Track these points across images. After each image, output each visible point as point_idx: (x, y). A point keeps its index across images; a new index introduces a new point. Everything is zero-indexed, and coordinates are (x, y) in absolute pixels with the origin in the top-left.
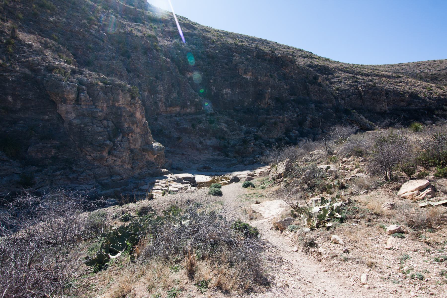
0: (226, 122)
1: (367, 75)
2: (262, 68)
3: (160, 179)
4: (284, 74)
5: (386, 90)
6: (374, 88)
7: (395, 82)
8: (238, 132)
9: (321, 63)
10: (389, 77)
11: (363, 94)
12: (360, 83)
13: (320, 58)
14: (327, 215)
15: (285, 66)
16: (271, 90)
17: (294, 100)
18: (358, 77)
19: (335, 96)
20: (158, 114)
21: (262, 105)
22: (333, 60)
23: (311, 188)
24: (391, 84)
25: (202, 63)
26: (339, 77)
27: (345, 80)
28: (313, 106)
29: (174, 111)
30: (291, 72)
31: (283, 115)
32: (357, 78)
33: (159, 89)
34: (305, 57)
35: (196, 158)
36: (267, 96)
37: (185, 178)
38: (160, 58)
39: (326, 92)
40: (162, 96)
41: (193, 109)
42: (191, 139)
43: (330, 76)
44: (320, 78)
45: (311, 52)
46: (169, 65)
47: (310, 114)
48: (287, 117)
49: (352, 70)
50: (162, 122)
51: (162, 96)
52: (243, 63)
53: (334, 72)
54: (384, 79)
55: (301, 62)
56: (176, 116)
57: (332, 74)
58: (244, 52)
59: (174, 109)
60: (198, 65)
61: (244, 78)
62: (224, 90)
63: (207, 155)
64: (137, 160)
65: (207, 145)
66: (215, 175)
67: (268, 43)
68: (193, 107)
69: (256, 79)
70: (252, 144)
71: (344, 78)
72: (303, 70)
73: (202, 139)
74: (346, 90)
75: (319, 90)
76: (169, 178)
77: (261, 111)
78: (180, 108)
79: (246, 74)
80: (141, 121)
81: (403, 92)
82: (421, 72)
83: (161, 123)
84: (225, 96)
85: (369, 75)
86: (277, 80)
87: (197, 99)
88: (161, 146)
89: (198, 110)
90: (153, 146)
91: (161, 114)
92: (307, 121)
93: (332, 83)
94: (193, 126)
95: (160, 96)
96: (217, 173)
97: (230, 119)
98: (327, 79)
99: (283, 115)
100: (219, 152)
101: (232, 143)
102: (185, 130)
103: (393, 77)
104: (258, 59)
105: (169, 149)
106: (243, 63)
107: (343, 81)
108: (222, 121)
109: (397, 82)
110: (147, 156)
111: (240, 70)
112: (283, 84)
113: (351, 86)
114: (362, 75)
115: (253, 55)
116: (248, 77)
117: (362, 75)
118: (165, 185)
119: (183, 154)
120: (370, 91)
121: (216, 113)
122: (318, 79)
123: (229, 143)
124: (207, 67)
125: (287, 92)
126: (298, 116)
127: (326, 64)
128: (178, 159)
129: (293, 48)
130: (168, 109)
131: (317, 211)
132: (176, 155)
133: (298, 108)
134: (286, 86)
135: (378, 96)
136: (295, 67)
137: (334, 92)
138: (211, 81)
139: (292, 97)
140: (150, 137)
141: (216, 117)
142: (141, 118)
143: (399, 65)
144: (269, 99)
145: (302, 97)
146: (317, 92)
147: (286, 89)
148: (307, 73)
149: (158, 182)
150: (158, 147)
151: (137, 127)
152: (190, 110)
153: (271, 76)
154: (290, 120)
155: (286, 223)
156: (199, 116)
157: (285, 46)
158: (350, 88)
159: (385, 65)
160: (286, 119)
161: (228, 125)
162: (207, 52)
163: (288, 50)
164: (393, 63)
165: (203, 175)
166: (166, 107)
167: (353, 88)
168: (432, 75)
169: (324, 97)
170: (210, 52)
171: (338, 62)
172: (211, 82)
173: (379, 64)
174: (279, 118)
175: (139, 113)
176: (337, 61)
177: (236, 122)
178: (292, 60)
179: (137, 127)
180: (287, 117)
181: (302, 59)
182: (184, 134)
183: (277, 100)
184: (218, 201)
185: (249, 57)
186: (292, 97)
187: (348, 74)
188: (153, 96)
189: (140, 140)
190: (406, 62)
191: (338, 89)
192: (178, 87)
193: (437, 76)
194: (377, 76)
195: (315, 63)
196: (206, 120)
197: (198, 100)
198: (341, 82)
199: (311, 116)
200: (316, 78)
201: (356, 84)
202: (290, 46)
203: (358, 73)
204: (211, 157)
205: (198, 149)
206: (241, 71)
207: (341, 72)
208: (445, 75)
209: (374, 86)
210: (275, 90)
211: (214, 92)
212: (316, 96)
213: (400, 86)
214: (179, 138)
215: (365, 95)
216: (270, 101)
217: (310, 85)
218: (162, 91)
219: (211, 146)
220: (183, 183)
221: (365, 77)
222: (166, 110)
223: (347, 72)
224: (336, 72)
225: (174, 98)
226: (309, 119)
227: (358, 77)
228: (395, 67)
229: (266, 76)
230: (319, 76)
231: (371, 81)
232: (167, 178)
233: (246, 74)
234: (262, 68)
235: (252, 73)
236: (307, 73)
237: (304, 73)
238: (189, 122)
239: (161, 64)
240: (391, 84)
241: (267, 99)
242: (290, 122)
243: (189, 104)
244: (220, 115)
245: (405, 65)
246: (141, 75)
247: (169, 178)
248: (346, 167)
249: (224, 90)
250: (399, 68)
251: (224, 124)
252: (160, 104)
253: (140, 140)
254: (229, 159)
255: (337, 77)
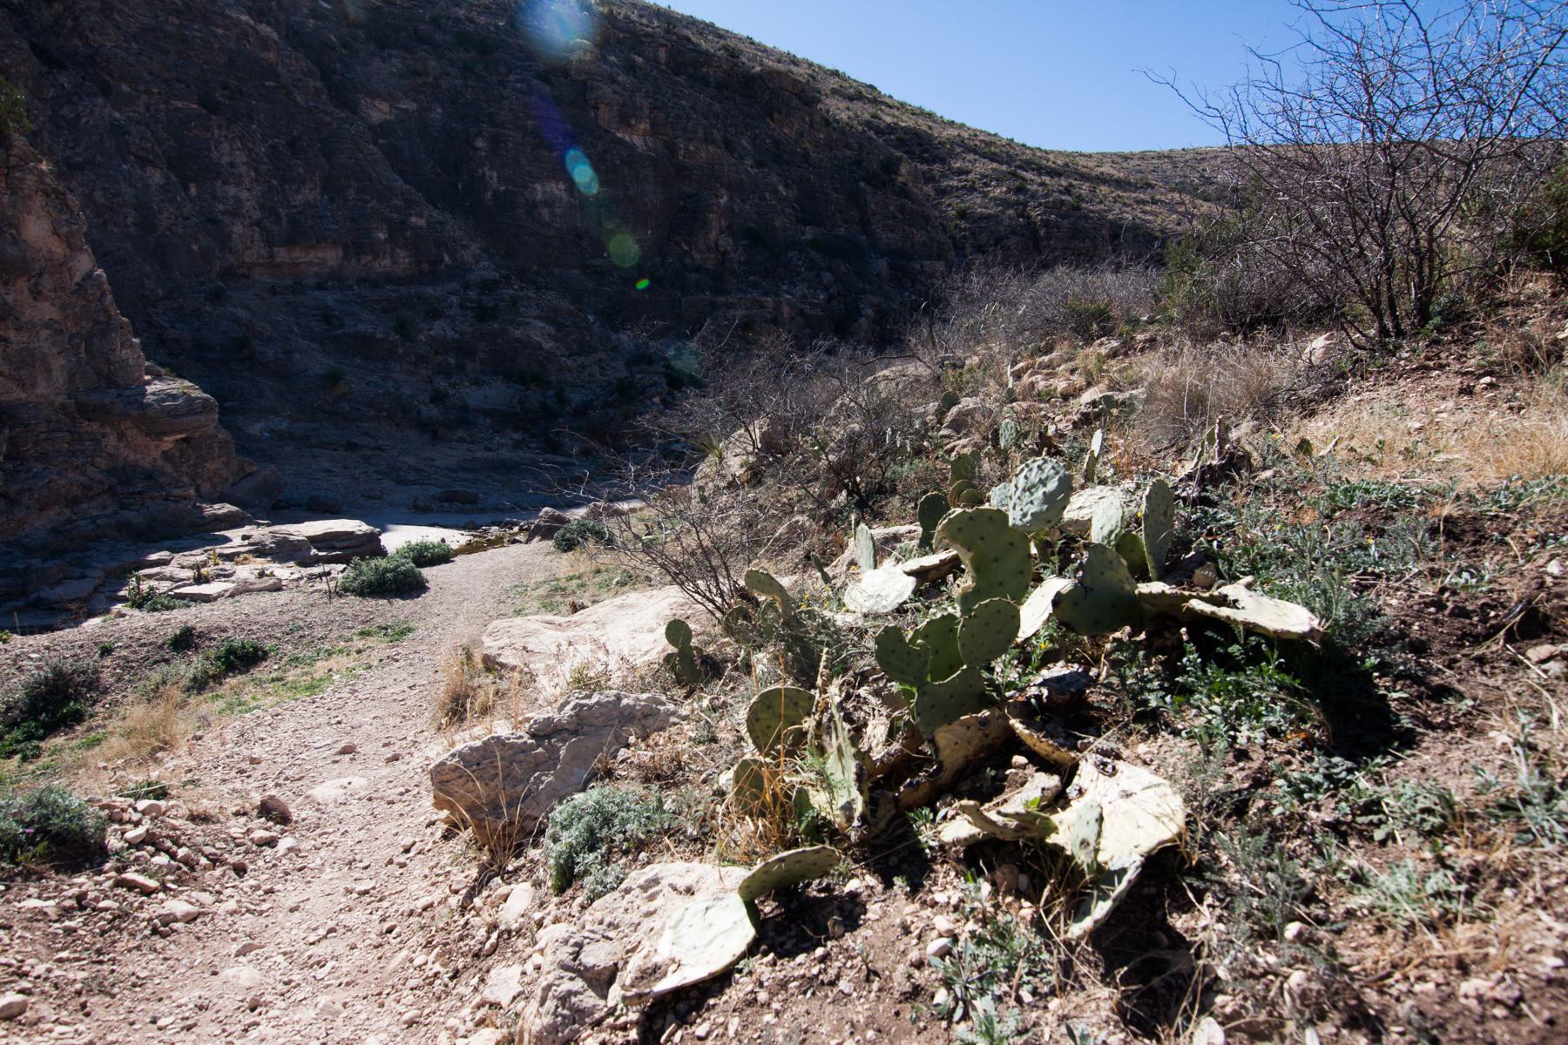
0: (551, 317)
1: (1054, 173)
2: (693, 108)
3: (174, 550)
4: (777, 143)
5: (1111, 223)
6: (1076, 213)
7: (1138, 202)
8: (602, 355)
9: (907, 122)
10: (1120, 184)
11: (1042, 232)
12: (1033, 196)
13: (903, 105)
14: (1035, 613)
15: (780, 112)
16: (731, 199)
17: (814, 244)
18: (1028, 175)
19: (953, 238)
20: (228, 274)
21: (697, 256)
22: (947, 118)
23: (862, 505)
24: (1125, 204)
25: (433, 64)
26: (968, 173)
27: (986, 185)
28: (882, 265)
29: (311, 263)
30: (801, 135)
31: (777, 295)
32: (1024, 179)
33: (226, 159)
34: (851, 99)
35: (411, 460)
36: (716, 223)
37: (314, 541)
38: (224, 16)
39: (927, 219)
40: (245, 195)
41: (404, 259)
42: (390, 384)
43: (937, 167)
44: (903, 170)
45: (871, 87)
46: (272, 56)
47: (872, 293)
48: (789, 303)
49: (1008, 155)
50: (247, 307)
51: (245, 195)
52: (613, 80)
53: (952, 154)
54: (1104, 189)
55: (839, 110)
56: (320, 287)
57: (943, 161)
58: (619, 41)
59: (311, 256)
60: (419, 74)
61: (621, 142)
62: (538, 187)
63: (466, 446)
64: (43, 457)
65: (465, 408)
66: (494, 524)
67: (721, 37)
68: (401, 253)
69: (671, 148)
70: (656, 400)
71: (983, 176)
72: (843, 133)
73: (442, 384)
74: (988, 217)
75: (902, 209)
76: (237, 541)
77: (694, 276)
78: (340, 253)
79: (629, 125)
80: (62, 265)
81: (1162, 231)
83: (242, 313)
84: (545, 213)
85: (1059, 175)
86: (749, 161)
87: (420, 215)
88: (197, 393)
89: (425, 266)
90: (144, 394)
91: (246, 277)
92: (862, 320)
93: (943, 192)
94: (402, 328)
95: (232, 191)
96: (499, 517)
97: (565, 305)
98: (929, 178)
99: (777, 295)
100: (518, 436)
101: (576, 398)
102: (365, 346)
103: (1129, 183)
104: (677, 74)
105: (284, 426)
106: (613, 80)
107: (978, 185)
108: (534, 312)
109: (1144, 202)
110: (111, 441)
111: (603, 108)
112: (775, 178)
113: (1005, 204)
114: (1039, 170)
115: (656, 60)
116: (637, 141)
117: (1039, 170)
118: (189, 573)
119: (352, 447)
120: (1065, 223)
121: (507, 278)
122: (897, 172)
123: (562, 400)
124: (459, 82)
125: (788, 211)
126: (829, 301)
127: (923, 125)
128: (326, 464)
129: (811, 65)
130: (282, 254)
131: (890, 603)
132: (315, 451)
133: (829, 269)
134: (787, 186)
135: (1088, 243)
136: (817, 118)
137: (952, 224)
138: (480, 143)
139: (809, 233)
140: (130, 350)
141: (507, 293)
142: (59, 249)
143: (1143, 156)
144: (722, 232)
145: (842, 231)
146: (895, 217)
148: (860, 145)
149: (165, 563)
150: (174, 397)
151: (36, 294)
152: (387, 262)
153: (729, 146)
154: (802, 312)
155: (550, 761)
156: (429, 290)
157: (781, 54)
158: (1003, 212)
159: (1104, 155)
160: (786, 310)
161: (560, 327)
162: (457, 20)
163: (792, 67)
164: (1126, 150)
165: (432, 525)
166: (270, 244)
167: (1011, 212)
169: (919, 237)
170: (471, 21)
171: (962, 126)
172: (476, 149)
173: (1086, 150)
174: (763, 307)
175: (47, 225)
176: (958, 121)
177: (591, 318)
178: (803, 91)
179: (36, 294)
180: (789, 303)
181: (843, 104)
182: (358, 360)
183: (755, 238)
184: (380, 621)
185: (640, 60)
186: (809, 233)
187: (995, 165)
188: (193, 190)
189: (58, 363)
190: (1164, 147)
191: (963, 215)
192: (322, 160)
194: (1084, 177)
195: (889, 119)
196: (461, 306)
197: (422, 222)
198: (972, 189)
199: (875, 300)
200: (890, 167)
201: (1022, 197)
202: (799, 56)
203: (1028, 165)
204: (481, 454)
205: (425, 426)
206: (604, 113)
207: (971, 157)
209: (1078, 208)
210: (743, 201)
211: (496, 193)
212: (892, 231)
213: (1151, 213)
214: (333, 378)
215: (1048, 236)
216: (726, 242)
217: (869, 189)
218: (243, 169)
219: (485, 413)
220: (304, 563)
221: (1047, 179)
222: (272, 256)
223: (993, 158)
224: (956, 156)
225: (307, 204)
226: (870, 312)
227: (1028, 175)
228: (1132, 163)
229: (708, 140)
230: (899, 160)
231: (1067, 191)
232: (228, 540)
233: (629, 125)
234: (693, 108)
235: (653, 125)
236: (860, 145)
237: (848, 146)
238: (384, 311)
239: (232, 45)
240: (1125, 204)
241: (715, 232)
242: (800, 320)
243: (382, 236)
244: (522, 289)
245: (1160, 156)
246: (125, 88)
247: (237, 541)
248: (1041, 385)
249: (538, 187)
250: (1143, 164)
251: (541, 324)
252: (238, 229)
253: (58, 363)
254: (561, 459)
255: (961, 172)
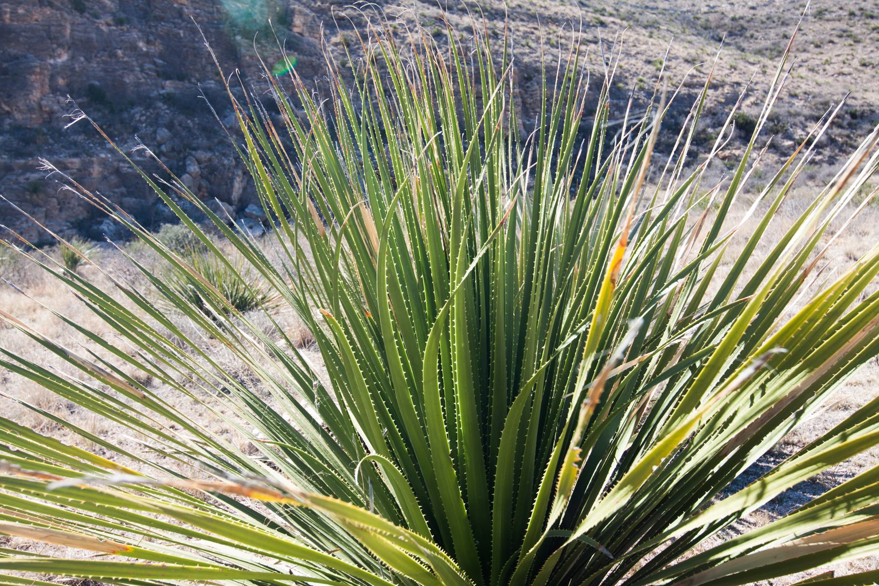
21: (18, 116)
82: (712, 9)
147: (147, 54)
168: (733, 19)
193: (746, 25)
208: (763, 22)
210: (88, 60)
